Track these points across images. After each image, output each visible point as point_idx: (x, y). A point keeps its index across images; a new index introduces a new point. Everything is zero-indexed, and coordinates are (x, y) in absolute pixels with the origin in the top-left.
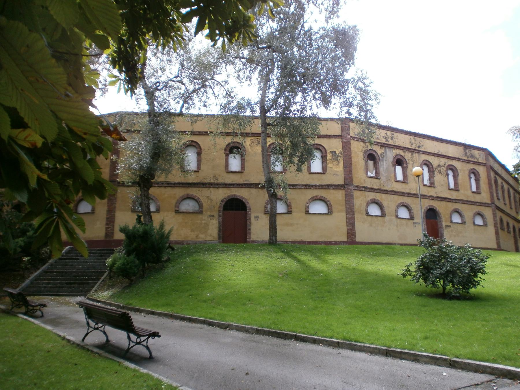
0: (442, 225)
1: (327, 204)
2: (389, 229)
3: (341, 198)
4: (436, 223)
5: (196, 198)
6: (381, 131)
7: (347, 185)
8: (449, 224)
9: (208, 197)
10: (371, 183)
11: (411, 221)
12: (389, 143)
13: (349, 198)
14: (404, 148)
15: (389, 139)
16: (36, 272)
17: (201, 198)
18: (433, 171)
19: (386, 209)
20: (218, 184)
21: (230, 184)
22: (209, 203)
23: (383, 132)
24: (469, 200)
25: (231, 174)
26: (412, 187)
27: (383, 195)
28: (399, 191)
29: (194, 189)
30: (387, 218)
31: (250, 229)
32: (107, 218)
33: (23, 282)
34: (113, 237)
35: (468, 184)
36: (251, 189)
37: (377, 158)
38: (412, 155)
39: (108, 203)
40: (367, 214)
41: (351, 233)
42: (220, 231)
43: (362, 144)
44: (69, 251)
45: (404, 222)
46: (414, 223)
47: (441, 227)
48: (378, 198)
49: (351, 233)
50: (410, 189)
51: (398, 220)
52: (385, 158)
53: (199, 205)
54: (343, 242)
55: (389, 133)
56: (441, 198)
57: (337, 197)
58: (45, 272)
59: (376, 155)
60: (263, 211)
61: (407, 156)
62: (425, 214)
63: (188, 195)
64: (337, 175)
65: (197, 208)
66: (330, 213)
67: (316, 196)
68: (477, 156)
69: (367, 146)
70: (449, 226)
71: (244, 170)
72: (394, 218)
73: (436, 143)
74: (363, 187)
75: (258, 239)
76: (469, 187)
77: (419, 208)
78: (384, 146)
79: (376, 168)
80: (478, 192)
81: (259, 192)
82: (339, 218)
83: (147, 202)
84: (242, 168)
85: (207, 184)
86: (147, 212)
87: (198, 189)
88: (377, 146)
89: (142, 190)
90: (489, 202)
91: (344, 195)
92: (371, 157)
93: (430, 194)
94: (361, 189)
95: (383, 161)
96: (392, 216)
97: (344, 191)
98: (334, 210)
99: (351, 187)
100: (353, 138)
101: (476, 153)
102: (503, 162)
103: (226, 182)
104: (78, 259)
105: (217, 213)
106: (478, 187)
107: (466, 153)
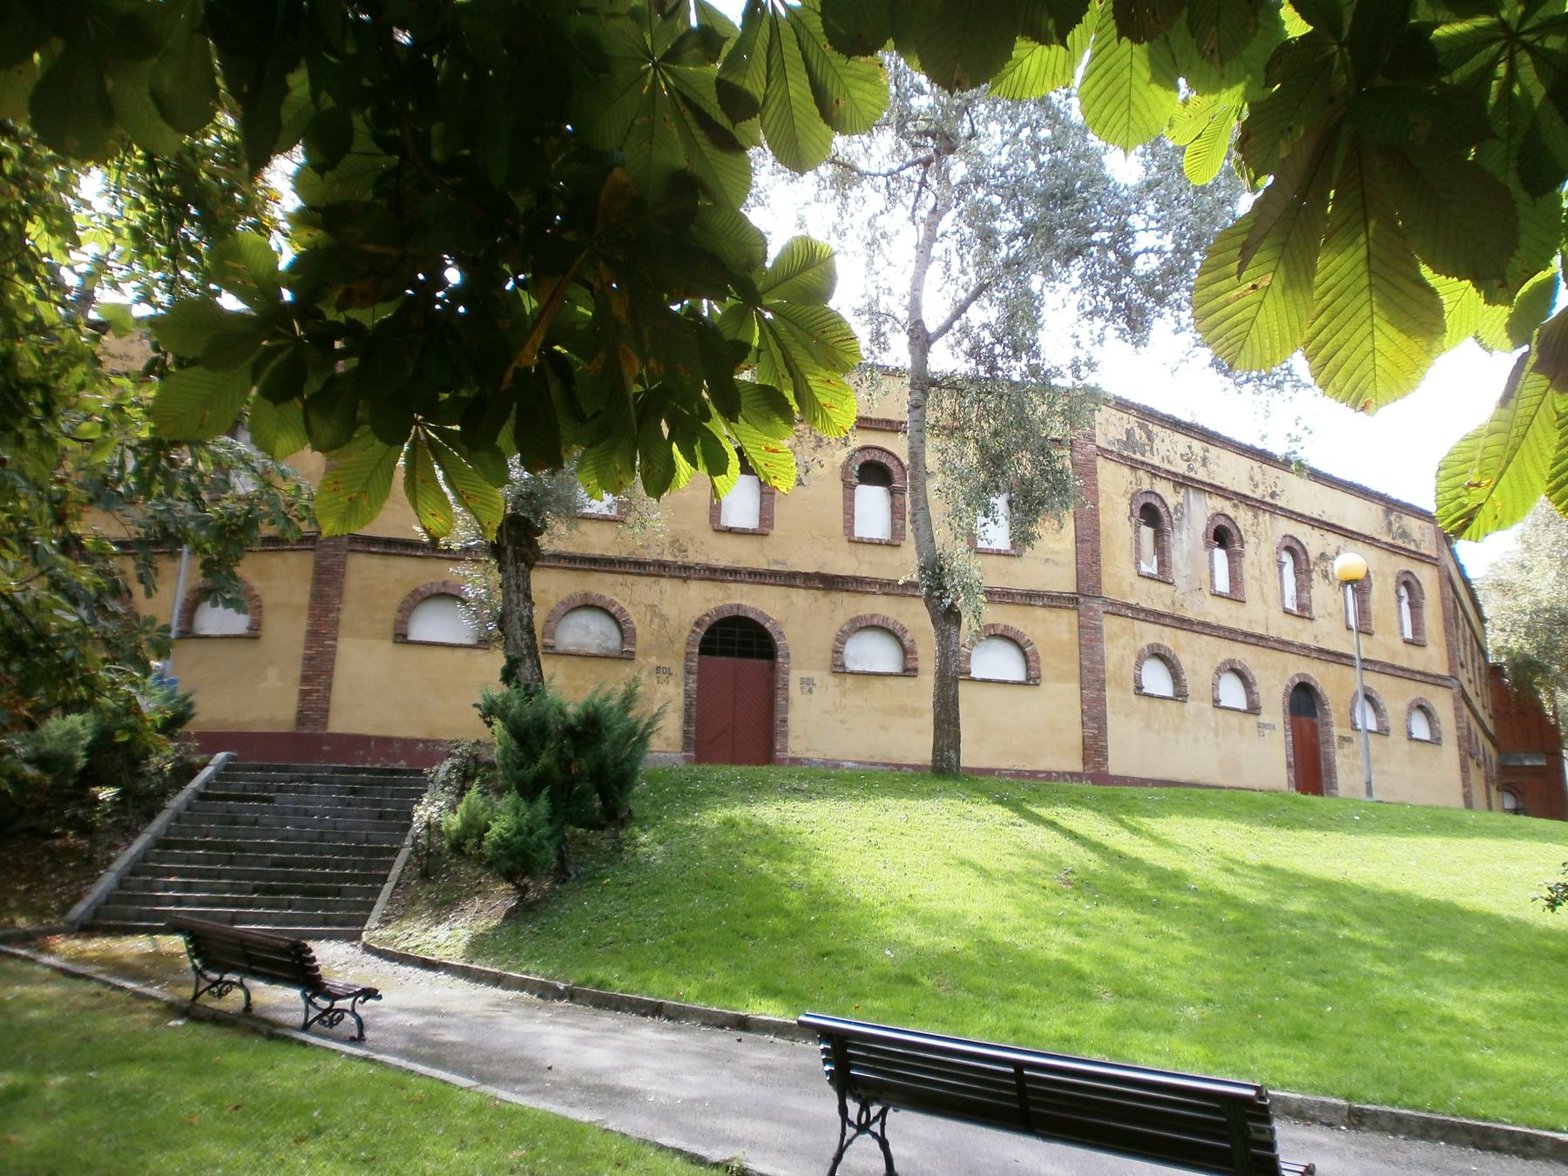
0: (1329, 734)
1: (1024, 654)
2: (1196, 740)
3: (1065, 636)
4: (1314, 727)
5: (613, 610)
6: (1179, 437)
7: (1083, 595)
8: (1348, 733)
9: (652, 608)
10: (1148, 594)
11: (1252, 720)
12: (1197, 477)
13: (1089, 640)
14: (1236, 494)
15: (1197, 465)
16: (130, 844)
17: (629, 610)
18: (1309, 571)
19: (1187, 676)
20: (686, 568)
21: (725, 571)
22: (655, 626)
23: (1182, 441)
24: (1397, 663)
25: (728, 538)
26: (1259, 614)
27: (1180, 632)
28: (1222, 624)
29: (609, 579)
30: (1191, 706)
31: (785, 721)
32: (308, 659)
33: (94, 878)
34: (325, 725)
35: (1395, 617)
36: (792, 591)
37: (1166, 519)
38: (1255, 517)
39: (312, 608)
40: (1139, 688)
41: (1094, 749)
42: (688, 720)
43: (1126, 471)
44: (227, 768)
45: (1234, 719)
46: (1259, 725)
47: (1328, 742)
48: (1167, 643)
49: (1094, 749)
50: (1250, 622)
51: (1220, 713)
52: (1185, 521)
53: (621, 631)
54: (1072, 774)
55: (1197, 446)
56: (1328, 652)
57: (1053, 630)
58: (163, 844)
59: (1162, 510)
60: (828, 663)
61: (1243, 518)
62: (1287, 700)
63: (586, 595)
64: (1056, 563)
65: (613, 641)
66: (1032, 679)
67: (993, 626)
68: (1416, 535)
69: (1139, 481)
70: (1348, 740)
71: (771, 526)
72: (1209, 705)
73: (1316, 487)
74: (1128, 606)
75: (809, 755)
76: (1396, 625)
77: (1275, 678)
78: (1183, 483)
79: (1161, 549)
80: (1416, 643)
81: (816, 600)
82: (1060, 699)
83: (526, 612)
84: (762, 519)
85: (649, 564)
86: (528, 647)
87: (619, 578)
88: (1164, 482)
89: (511, 569)
90: (1445, 673)
91: (1076, 628)
92: (1150, 515)
93: (1300, 640)
94: (1123, 611)
95: (1180, 529)
96: (1202, 700)
97: (1074, 614)
98: (1044, 672)
99: (1096, 604)
100: (1103, 452)
101: (1413, 524)
102: (1462, 561)
103: (713, 563)
104: (270, 800)
105: (682, 662)
106: (1417, 627)
107: (1390, 524)
